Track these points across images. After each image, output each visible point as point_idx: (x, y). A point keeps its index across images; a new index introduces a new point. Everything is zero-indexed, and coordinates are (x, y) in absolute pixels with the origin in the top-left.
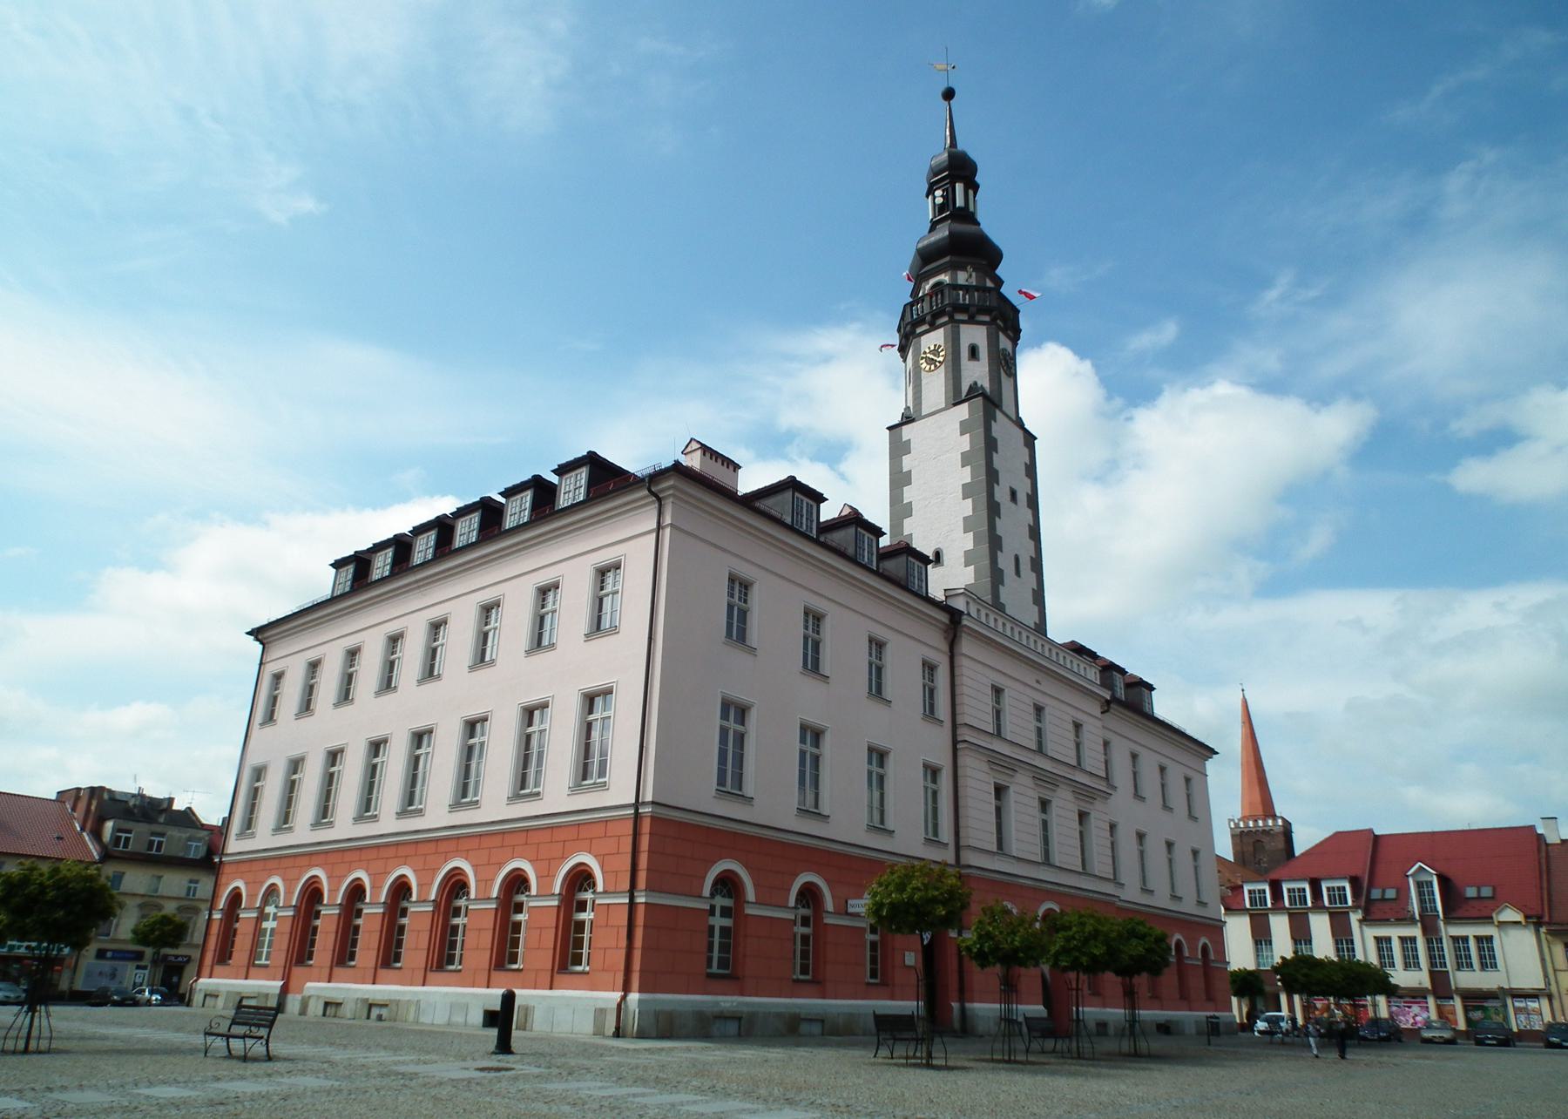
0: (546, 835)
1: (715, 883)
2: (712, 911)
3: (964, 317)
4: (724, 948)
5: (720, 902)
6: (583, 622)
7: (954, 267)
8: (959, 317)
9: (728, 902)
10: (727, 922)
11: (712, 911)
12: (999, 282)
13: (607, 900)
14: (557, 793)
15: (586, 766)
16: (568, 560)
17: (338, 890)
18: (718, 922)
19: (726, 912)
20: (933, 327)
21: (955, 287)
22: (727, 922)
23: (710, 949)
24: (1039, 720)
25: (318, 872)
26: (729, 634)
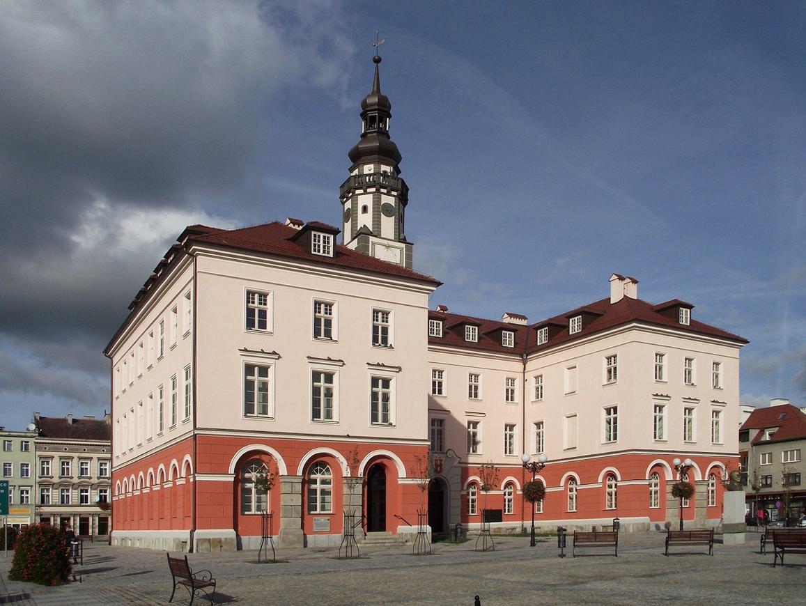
2: (650, 485)
5: (653, 481)
11: (650, 485)
17: (358, 462)
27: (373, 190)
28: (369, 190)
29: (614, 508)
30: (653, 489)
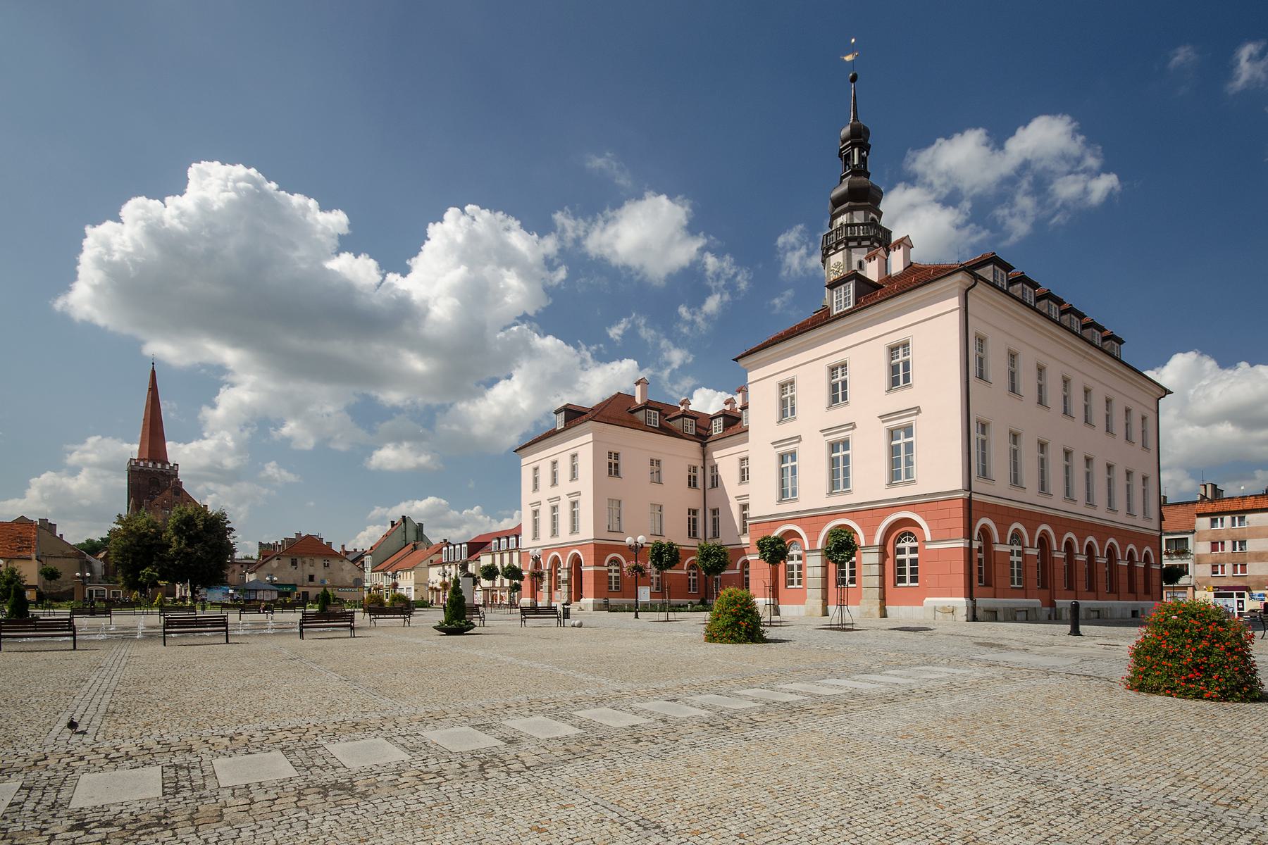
0: (564, 548)
1: (1012, 537)
2: (1012, 553)
3: (855, 244)
4: (1019, 573)
5: (613, 568)
6: (549, 482)
7: (850, 210)
8: (851, 244)
9: (1020, 548)
10: (1020, 559)
11: (610, 571)
12: (880, 214)
13: (588, 569)
14: (565, 536)
15: (984, 448)
16: (560, 451)
17: (874, 535)
18: (613, 574)
19: (616, 571)
20: (837, 251)
21: (852, 225)
22: (1020, 559)
23: (1013, 573)
24: (1015, 443)
25: (576, 551)
26: (610, 473)
27: (868, 243)
28: (864, 243)
29: (908, 583)
30: (691, 577)
